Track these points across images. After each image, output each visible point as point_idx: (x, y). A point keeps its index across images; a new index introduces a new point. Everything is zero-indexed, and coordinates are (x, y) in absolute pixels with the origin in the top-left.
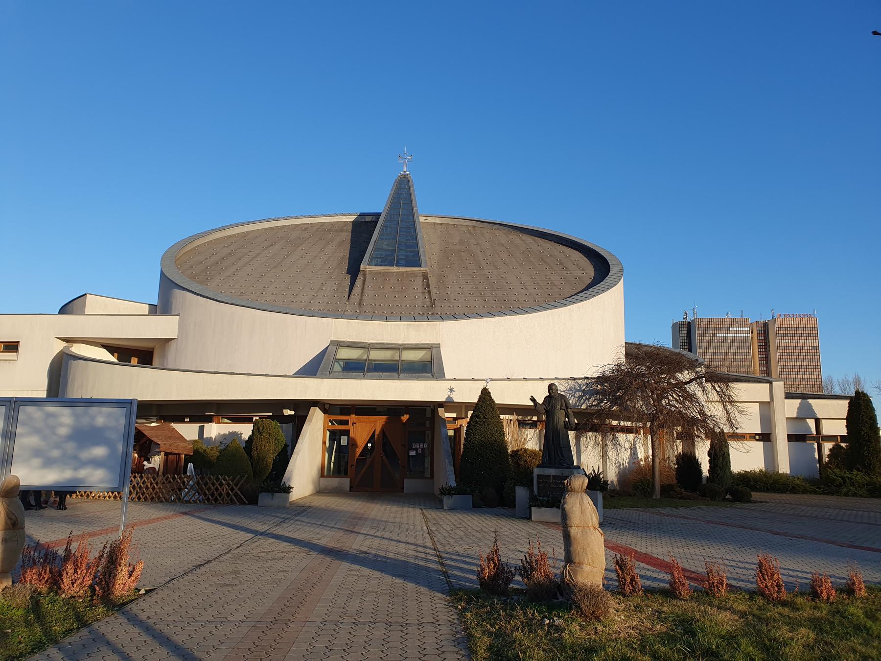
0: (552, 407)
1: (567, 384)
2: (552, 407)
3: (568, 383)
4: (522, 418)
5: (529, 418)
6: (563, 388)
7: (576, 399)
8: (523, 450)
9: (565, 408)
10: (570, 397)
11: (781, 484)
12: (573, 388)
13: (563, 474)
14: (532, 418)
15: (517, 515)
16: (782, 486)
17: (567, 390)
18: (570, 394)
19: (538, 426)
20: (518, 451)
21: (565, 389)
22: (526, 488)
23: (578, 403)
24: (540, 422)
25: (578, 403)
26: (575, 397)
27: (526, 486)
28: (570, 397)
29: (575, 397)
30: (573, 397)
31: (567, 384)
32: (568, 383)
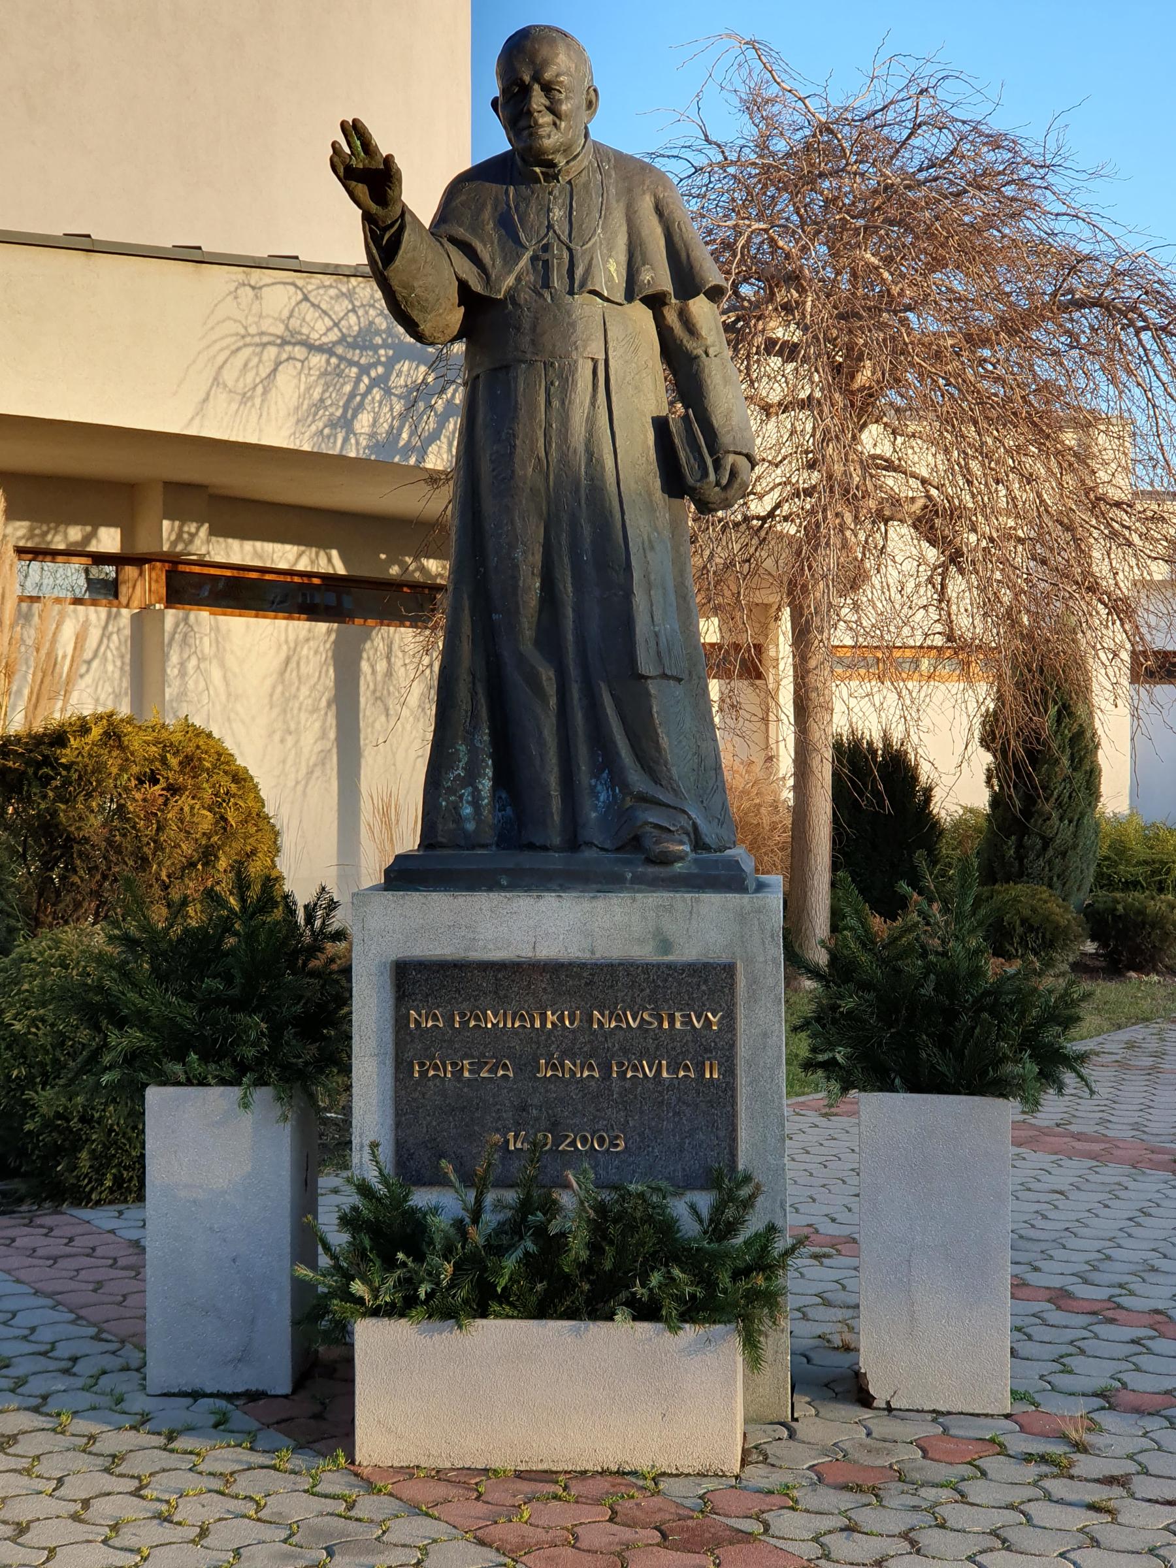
0: (542, 265)
1: (346, 304)
2: (542, 265)
3: (350, 295)
4: (31, 536)
5: (75, 534)
6: (321, 326)
7: (398, 407)
8: (96, 732)
9: (658, 276)
10: (362, 387)
11: (1139, 864)
12: (378, 332)
13: (666, 945)
14: (93, 535)
15: (159, 1374)
16: (1140, 870)
17: (343, 339)
18: (364, 370)
19: (123, 590)
20: (58, 738)
21: (334, 336)
22: (263, 1094)
23: (405, 436)
24: (139, 561)
25: (405, 436)
26: (388, 392)
27: (261, 1082)
28: (362, 387)
29: (388, 392)
30: (377, 393)
31: (346, 304)
32: (350, 295)
